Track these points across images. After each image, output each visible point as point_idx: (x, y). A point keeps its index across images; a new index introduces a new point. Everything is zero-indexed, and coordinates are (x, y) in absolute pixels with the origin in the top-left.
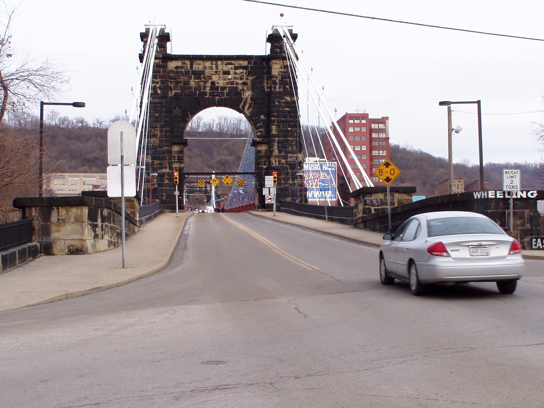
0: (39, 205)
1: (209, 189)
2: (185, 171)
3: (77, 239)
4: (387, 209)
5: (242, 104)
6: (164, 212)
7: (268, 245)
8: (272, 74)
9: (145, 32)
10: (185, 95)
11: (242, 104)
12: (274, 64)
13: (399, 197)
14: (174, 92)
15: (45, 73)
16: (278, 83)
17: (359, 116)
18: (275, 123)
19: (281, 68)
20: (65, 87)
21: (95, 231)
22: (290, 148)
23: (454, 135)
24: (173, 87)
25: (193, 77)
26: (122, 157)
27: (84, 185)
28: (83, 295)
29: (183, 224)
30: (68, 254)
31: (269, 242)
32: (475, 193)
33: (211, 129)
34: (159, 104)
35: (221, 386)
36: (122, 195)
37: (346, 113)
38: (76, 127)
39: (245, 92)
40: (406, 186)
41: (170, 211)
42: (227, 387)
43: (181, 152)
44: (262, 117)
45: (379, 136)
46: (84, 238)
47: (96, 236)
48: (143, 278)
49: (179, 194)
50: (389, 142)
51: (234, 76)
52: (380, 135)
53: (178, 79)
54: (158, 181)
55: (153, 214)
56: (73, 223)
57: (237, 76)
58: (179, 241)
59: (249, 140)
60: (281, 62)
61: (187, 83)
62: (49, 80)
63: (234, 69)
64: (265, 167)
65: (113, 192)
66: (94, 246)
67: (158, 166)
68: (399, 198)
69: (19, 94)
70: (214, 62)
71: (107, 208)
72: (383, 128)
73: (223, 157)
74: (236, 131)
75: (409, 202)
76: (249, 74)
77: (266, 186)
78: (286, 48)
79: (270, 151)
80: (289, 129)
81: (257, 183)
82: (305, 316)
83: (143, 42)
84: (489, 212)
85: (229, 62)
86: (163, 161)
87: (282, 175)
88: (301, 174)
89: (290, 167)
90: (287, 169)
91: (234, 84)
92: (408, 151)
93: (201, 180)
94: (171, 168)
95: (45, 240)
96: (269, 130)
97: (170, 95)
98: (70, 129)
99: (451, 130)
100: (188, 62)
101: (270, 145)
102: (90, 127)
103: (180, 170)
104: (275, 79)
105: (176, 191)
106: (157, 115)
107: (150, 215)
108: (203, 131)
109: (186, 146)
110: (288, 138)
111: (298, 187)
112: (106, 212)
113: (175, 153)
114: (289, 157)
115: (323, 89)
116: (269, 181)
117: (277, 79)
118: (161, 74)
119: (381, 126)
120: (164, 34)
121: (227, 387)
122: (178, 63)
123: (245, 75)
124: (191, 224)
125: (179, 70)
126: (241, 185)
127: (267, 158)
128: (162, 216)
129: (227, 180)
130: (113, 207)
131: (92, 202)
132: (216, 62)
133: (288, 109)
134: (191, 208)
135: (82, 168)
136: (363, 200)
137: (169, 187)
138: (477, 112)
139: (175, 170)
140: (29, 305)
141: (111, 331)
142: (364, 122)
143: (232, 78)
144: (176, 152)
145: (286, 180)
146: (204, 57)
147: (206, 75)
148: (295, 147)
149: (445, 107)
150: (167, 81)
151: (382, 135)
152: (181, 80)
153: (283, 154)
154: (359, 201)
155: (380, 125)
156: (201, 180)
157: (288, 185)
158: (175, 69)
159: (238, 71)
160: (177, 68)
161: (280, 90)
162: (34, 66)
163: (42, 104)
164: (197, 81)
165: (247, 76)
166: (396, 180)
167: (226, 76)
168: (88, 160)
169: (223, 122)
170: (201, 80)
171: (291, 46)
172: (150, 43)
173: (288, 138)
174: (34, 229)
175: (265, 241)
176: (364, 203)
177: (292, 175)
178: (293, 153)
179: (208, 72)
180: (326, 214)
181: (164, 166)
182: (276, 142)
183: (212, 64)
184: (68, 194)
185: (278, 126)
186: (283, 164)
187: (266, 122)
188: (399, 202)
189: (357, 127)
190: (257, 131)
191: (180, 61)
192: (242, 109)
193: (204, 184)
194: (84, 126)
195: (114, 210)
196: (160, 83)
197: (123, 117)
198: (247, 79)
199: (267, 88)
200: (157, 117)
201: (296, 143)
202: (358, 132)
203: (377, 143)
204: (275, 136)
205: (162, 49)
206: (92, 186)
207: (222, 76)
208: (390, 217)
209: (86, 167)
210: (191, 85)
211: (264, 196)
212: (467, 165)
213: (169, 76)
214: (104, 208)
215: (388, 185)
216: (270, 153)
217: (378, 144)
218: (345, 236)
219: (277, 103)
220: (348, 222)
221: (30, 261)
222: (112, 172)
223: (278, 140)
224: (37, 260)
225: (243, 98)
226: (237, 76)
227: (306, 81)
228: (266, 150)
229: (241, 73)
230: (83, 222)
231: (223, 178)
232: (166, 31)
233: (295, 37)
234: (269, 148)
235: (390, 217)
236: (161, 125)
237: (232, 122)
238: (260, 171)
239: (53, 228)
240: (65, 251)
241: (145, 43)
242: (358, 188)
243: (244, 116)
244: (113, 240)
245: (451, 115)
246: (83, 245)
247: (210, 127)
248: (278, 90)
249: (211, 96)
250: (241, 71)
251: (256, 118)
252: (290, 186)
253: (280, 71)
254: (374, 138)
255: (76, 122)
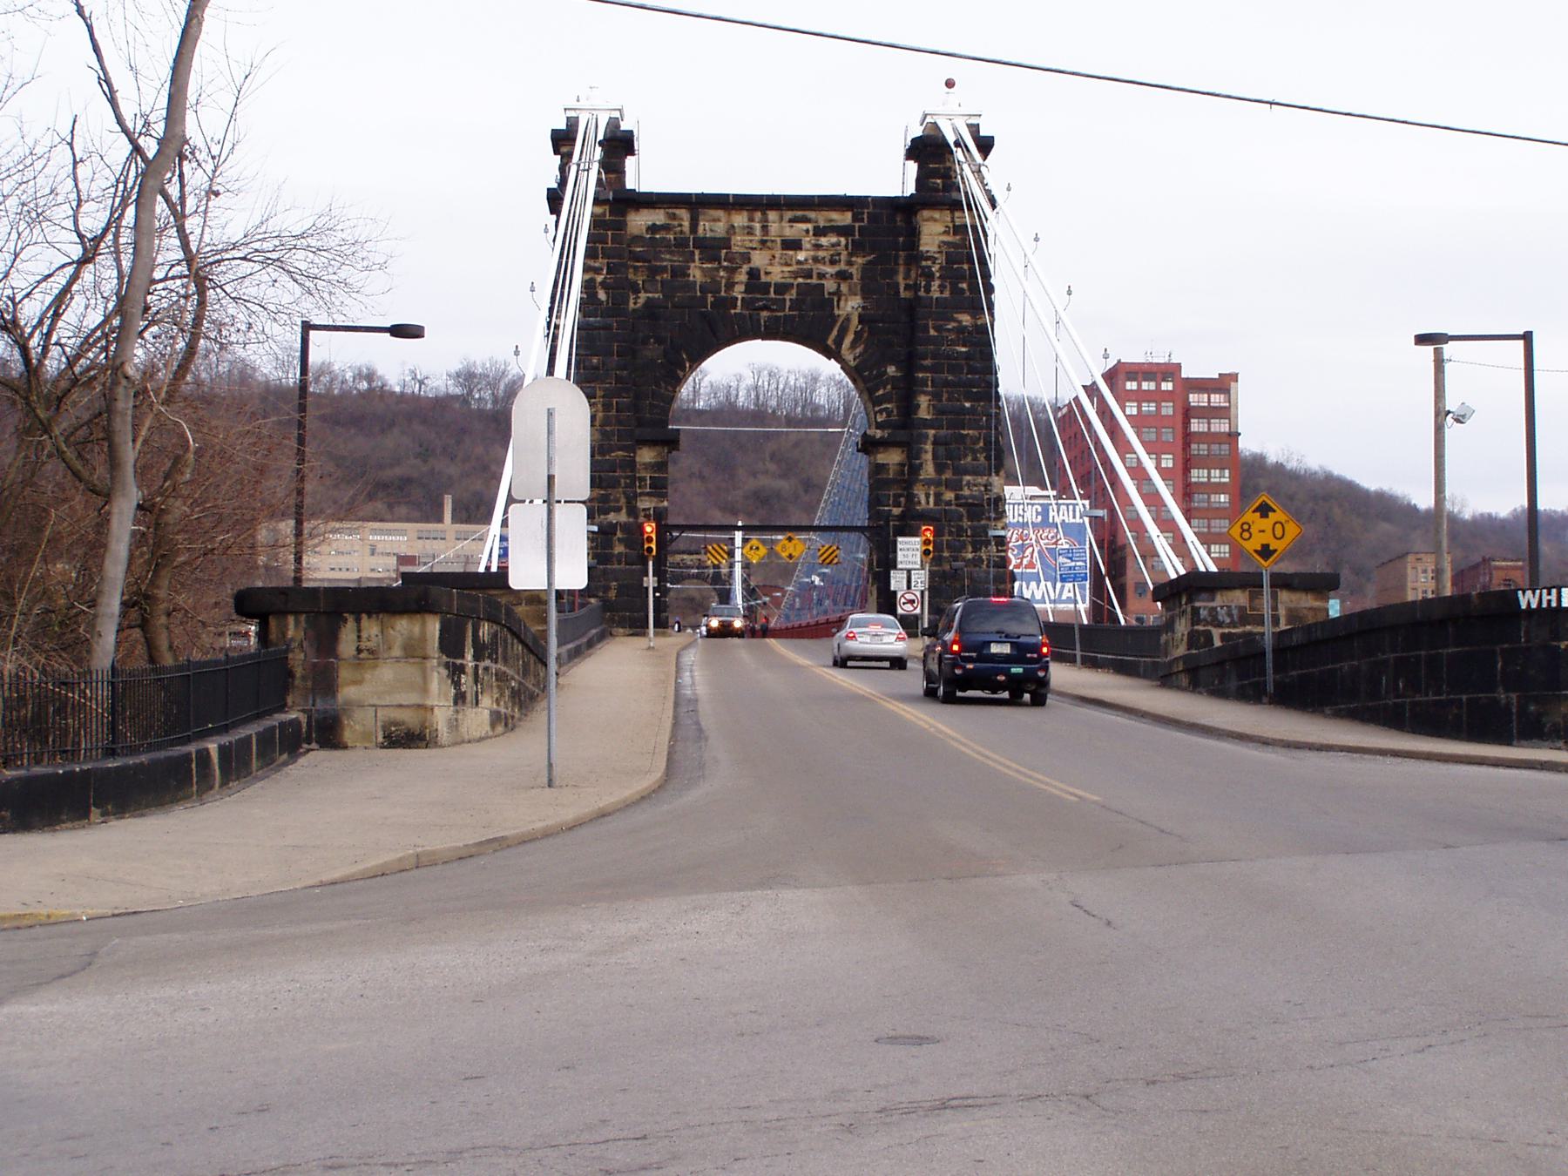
0: (307, 609)
1: (724, 571)
2: (672, 521)
3: (408, 706)
4: (1263, 634)
5: (835, 332)
6: (611, 634)
7: (932, 730)
8: (921, 248)
9: (564, 127)
10: (674, 306)
11: (835, 332)
12: (927, 220)
13: (1291, 601)
14: (643, 296)
15: (320, 243)
16: (938, 275)
17: (1155, 369)
18: (927, 386)
19: (946, 233)
20: (376, 281)
21: (457, 684)
22: (969, 458)
23: (1452, 430)
24: (640, 282)
25: (697, 257)
26: (551, 478)
27: (373, 554)
28: (460, 858)
29: (674, 668)
30: (383, 747)
31: (932, 721)
32: (1524, 594)
33: (730, 403)
34: (602, 332)
35: (954, 1099)
36: (550, 583)
37: (1115, 362)
38: (351, 392)
39: (843, 298)
40: (1283, 571)
41: (628, 631)
42: (970, 1102)
43: (661, 466)
44: (891, 370)
45: (1209, 428)
46: (429, 703)
47: (460, 698)
48: (610, 814)
49: (656, 585)
50: (1240, 446)
51: (812, 253)
52: (1212, 426)
53: (655, 260)
54: (596, 548)
55: (585, 640)
56: (398, 660)
57: (821, 254)
58: (675, 717)
59: (851, 434)
60: (947, 216)
61: (680, 272)
62: (332, 262)
63: (814, 235)
64: (896, 511)
65: (526, 575)
66: (454, 725)
67: (597, 505)
68: (1292, 606)
69: (248, 301)
70: (758, 215)
71: (488, 620)
72: (1222, 404)
73: (764, 481)
74: (803, 407)
75: (1321, 618)
76: (857, 248)
77: (899, 566)
78: (962, 178)
79: (911, 466)
80: (967, 405)
81: (875, 557)
82: (1109, 923)
83: (559, 157)
84: (1563, 647)
85: (799, 213)
86: (610, 491)
87: (943, 536)
88: (1002, 533)
89: (968, 512)
90: (960, 518)
91: (811, 277)
92: (1291, 470)
93: (715, 546)
94: (633, 511)
95: (320, 705)
96: (909, 407)
97: (631, 305)
98: (334, 397)
99: (1443, 414)
100: (684, 214)
101: (911, 449)
102: (393, 393)
103: (659, 516)
104: (929, 263)
105: (647, 575)
106: (595, 361)
107: (577, 643)
108: (708, 409)
109: (674, 449)
110: (962, 432)
111: (992, 569)
112: (486, 632)
113: (646, 469)
114: (964, 483)
115: (1069, 293)
116: (910, 550)
117: (934, 263)
118: (610, 245)
119: (1217, 399)
120: (619, 134)
121: (970, 1102)
122: (656, 217)
123: (845, 252)
124: (694, 668)
125: (658, 236)
126: (828, 561)
127: (904, 485)
128: (607, 647)
129: (793, 547)
130: (503, 617)
131: (451, 606)
132: (764, 214)
133: (964, 349)
134: (678, 623)
135: (369, 508)
136: (1189, 609)
137: (626, 564)
138: (1522, 366)
139: (645, 516)
140: (322, 882)
141: (590, 954)
142: (1167, 386)
143: (806, 260)
144: (647, 466)
145: (957, 549)
146: (731, 198)
147: (735, 249)
148: (981, 457)
149: (1428, 350)
150: (627, 267)
151: (1221, 426)
152: (665, 264)
153: (948, 476)
154: (1177, 611)
155: (1212, 396)
156: (715, 546)
157: (963, 563)
158: (647, 233)
159: (824, 241)
160: (653, 228)
161: (944, 296)
162: (292, 222)
163: (307, 327)
164: (709, 266)
165: (851, 255)
166: (1290, 554)
167: (791, 253)
168: (383, 486)
169: (766, 383)
170: (720, 263)
171: (978, 172)
172: (580, 159)
173: (964, 429)
174: (291, 674)
175: (921, 719)
176: (1192, 619)
177: (972, 536)
178: (975, 472)
179: (739, 242)
180: (1078, 646)
181: (612, 504)
182: (929, 442)
183: (751, 219)
184: (329, 580)
185: (936, 396)
186: (949, 503)
187: (902, 385)
188: (1293, 615)
189: (1149, 401)
190: (877, 409)
191: (662, 211)
192: (833, 347)
193: (723, 558)
194: (374, 389)
195: (507, 627)
196: (605, 272)
197: (484, 364)
198: (850, 263)
199: (907, 287)
200: (596, 368)
201: (985, 444)
202: (1149, 415)
203: (1205, 447)
204: (926, 424)
205: (613, 176)
206: (395, 558)
207: (778, 253)
208: (1269, 656)
209: (379, 506)
210: (691, 278)
211: (895, 593)
212: (1460, 512)
213: (630, 252)
214: (482, 619)
215: (1267, 567)
216: (910, 471)
217: (1208, 450)
218: (1144, 709)
219: (932, 332)
220: (1142, 670)
221: (285, 764)
222: (526, 521)
223: (935, 436)
224: (302, 761)
225: (839, 316)
226: (821, 254)
227: (1020, 270)
228: (902, 465)
229: (833, 245)
230: (424, 658)
231: (780, 540)
232: (624, 126)
233: (985, 145)
234: (908, 457)
235: (1269, 656)
236: (605, 390)
237: (792, 383)
238: (882, 523)
239: (344, 674)
240: (376, 738)
241: (566, 159)
242: (1173, 576)
243: (839, 366)
244: (503, 710)
245: (1444, 372)
246: (425, 722)
247: (728, 396)
248: (936, 295)
249: (747, 309)
250: (834, 239)
251: (875, 372)
252: (966, 566)
253: (945, 243)
254: (1195, 433)
255: (354, 378)
